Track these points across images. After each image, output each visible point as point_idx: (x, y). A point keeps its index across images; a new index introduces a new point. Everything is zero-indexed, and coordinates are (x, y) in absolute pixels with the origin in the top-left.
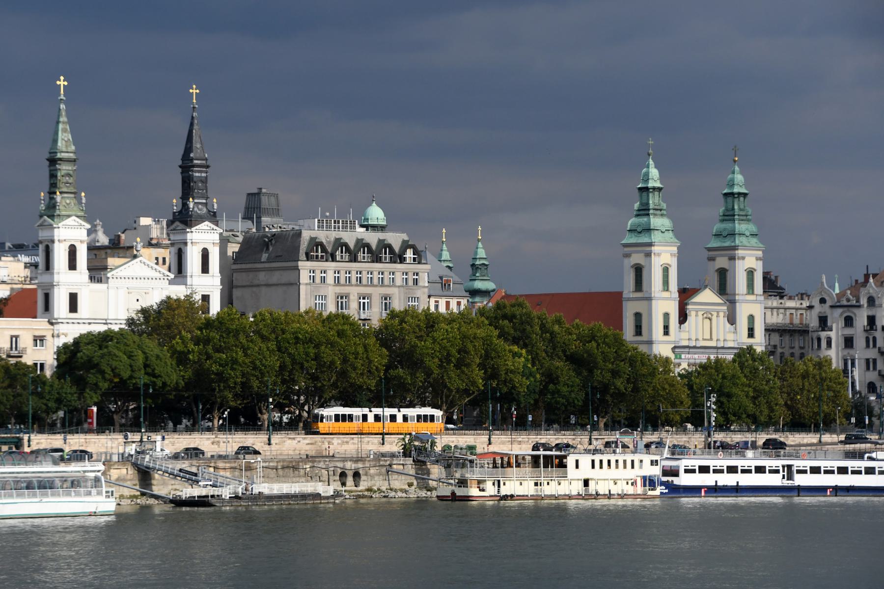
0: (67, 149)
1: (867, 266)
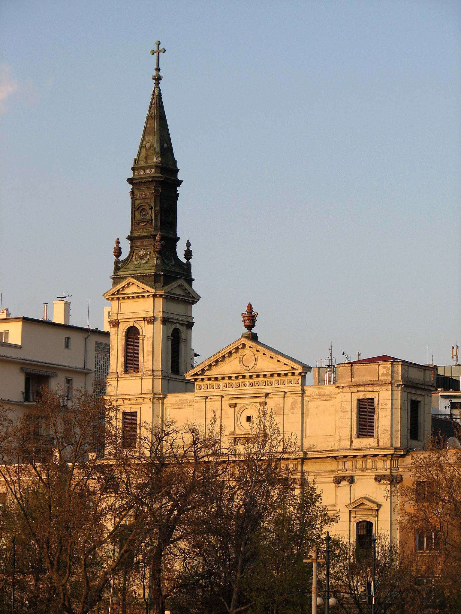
0: (146, 162)
1: (67, 346)
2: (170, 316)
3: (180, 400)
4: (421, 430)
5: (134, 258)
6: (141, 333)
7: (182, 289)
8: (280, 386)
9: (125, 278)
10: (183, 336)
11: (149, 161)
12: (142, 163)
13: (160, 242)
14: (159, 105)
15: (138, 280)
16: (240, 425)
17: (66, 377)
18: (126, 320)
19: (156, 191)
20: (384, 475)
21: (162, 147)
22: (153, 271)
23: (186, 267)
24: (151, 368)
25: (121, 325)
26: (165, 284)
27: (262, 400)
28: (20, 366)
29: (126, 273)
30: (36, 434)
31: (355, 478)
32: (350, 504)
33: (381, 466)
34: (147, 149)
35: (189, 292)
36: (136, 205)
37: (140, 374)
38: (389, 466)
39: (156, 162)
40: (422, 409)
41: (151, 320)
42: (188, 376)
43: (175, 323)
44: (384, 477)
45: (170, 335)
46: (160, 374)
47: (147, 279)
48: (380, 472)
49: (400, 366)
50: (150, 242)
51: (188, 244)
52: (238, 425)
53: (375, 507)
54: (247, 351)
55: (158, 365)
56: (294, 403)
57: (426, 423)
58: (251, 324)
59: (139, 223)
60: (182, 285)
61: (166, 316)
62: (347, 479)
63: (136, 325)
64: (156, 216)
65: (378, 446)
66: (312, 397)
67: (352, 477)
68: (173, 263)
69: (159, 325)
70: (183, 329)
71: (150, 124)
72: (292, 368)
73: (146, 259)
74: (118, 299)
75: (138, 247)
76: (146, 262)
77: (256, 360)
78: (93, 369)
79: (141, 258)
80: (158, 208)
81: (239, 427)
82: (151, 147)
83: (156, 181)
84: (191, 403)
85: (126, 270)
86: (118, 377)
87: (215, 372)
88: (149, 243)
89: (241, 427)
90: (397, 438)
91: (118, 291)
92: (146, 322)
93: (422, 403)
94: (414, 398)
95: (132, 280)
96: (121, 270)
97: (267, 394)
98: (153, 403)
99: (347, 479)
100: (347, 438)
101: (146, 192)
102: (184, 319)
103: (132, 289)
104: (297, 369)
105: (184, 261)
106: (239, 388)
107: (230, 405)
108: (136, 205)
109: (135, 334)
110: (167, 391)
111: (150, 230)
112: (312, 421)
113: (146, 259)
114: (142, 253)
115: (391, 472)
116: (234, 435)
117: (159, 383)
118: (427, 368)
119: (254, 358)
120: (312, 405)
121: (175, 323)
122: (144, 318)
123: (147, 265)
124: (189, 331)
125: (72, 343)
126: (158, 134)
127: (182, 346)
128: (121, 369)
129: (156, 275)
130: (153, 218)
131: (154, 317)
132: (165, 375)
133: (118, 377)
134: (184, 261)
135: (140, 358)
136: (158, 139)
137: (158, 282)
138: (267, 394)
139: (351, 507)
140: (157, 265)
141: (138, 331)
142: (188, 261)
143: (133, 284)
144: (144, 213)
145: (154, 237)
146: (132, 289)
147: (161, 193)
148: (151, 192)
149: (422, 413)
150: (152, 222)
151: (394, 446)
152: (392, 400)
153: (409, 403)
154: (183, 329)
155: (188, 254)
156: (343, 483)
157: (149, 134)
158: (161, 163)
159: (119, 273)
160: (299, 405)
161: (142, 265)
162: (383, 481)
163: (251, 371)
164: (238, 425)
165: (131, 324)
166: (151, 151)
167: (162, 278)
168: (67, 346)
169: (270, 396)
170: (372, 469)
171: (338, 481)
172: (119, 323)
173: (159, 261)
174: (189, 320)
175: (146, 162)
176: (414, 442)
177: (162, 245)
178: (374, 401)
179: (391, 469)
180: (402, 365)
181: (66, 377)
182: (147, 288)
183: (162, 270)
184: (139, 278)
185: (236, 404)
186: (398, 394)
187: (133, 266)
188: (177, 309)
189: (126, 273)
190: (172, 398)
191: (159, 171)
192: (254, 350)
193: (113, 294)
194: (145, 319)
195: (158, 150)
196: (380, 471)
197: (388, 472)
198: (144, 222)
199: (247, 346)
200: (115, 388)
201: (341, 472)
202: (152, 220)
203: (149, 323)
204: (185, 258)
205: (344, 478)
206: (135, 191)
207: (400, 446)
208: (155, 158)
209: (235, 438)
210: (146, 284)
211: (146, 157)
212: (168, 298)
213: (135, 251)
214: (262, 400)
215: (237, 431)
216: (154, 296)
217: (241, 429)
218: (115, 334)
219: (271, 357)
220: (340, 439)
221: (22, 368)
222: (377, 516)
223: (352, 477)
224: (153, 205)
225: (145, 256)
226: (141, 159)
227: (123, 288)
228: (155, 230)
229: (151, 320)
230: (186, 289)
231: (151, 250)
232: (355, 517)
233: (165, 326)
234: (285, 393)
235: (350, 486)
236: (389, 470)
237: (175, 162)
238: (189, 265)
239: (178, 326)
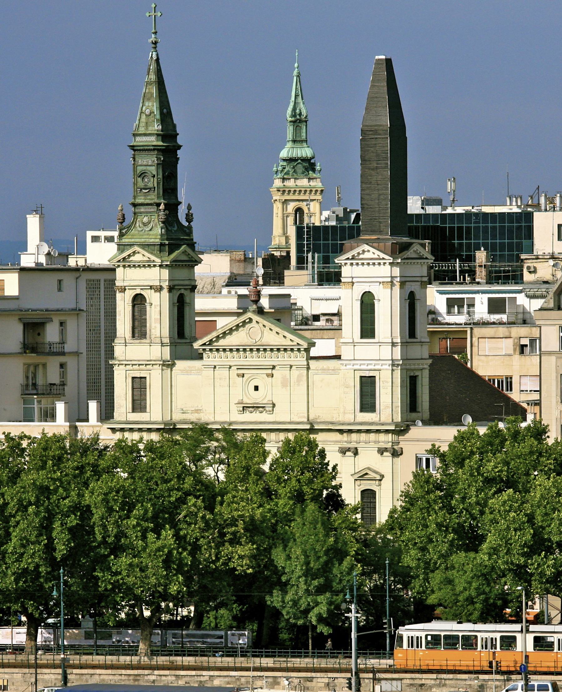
0: (147, 129)
1: (60, 290)
2: (176, 283)
3: (189, 367)
4: (419, 400)
5: (137, 225)
6: (148, 301)
7: (186, 255)
8: (286, 359)
9: (131, 245)
10: (187, 300)
11: (150, 128)
12: (143, 129)
13: (164, 211)
14: (158, 69)
15: (143, 249)
16: (248, 394)
17: (60, 320)
18: (133, 287)
19: (158, 159)
20: (386, 448)
21: (161, 113)
22: (158, 241)
23: (188, 231)
24: (158, 335)
25: (127, 291)
26: (170, 253)
27: (269, 371)
28: (17, 318)
29: (130, 240)
30: (34, 385)
31: (359, 451)
32: (355, 473)
33: (383, 440)
34: (146, 115)
35: (192, 257)
36: (138, 172)
37: (148, 341)
38: (390, 440)
39: (158, 130)
40: (420, 382)
41: (160, 289)
42: (196, 345)
43: (180, 289)
44: (386, 450)
45: (176, 301)
46: (168, 342)
47: (152, 247)
48: (383, 445)
49: (399, 347)
50: (154, 209)
51: (189, 207)
52: (245, 394)
53: (378, 477)
54: (254, 324)
55: (166, 332)
56: (299, 376)
57: (423, 403)
58: (257, 299)
59: (141, 189)
60: (185, 251)
61: (172, 283)
62: (352, 450)
63: (143, 292)
64: (158, 183)
65: (380, 420)
66: (317, 371)
67: (356, 449)
68: (176, 228)
69: (165, 294)
70: (186, 293)
71: (149, 89)
72: (298, 344)
73: (150, 226)
74: (124, 266)
75: (141, 213)
76: (151, 230)
77: (262, 333)
78: (85, 310)
79: (145, 224)
80: (160, 176)
81: (246, 395)
82: (151, 113)
83: (158, 150)
84: (200, 370)
85: (130, 237)
86: (126, 343)
87: (222, 343)
88: (152, 210)
89: (248, 394)
90: (397, 414)
91: (124, 259)
92: (153, 291)
93: (420, 377)
94: (412, 374)
95: (136, 248)
96: (124, 237)
97: (274, 367)
98: (162, 370)
99: (352, 450)
100: (351, 412)
101: (148, 160)
102: (187, 283)
103: (137, 258)
104: (302, 346)
105: (186, 224)
106: (246, 359)
107: (238, 375)
108: (138, 172)
109: (141, 301)
110: (176, 356)
111: (153, 198)
112: (317, 394)
113: (150, 226)
114: (145, 220)
115: (392, 445)
116: (242, 403)
117: (167, 350)
118: (424, 344)
119: (260, 331)
120: (315, 377)
121: (180, 289)
122: (151, 286)
123: (151, 233)
124: (192, 294)
125: (65, 284)
126: (158, 100)
127: (187, 310)
128: (128, 334)
129: (162, 245)
130: (156, 185)
131: (161, 286)
132: (173, 341)
133: (126, 343)
134: (186, 224)
135: (148, 325)
136: (158, 106)
137: (163, 251)
138: (274, 367)
139: (356, 477)
140: (162, 235)
141: (145, 298)
142: (189, 224)
143: (138, 253)
144: (146, 180)
145: (158, 205)
146: (137, 258)
147: (163, 161)
148: (153, 159)
149: (420, 386)
150: (154, 190)
151: (395, 421)
152: (392, 378)
153: (408, 380)
154: (186, 293)
155: (189, 218)
156: (348, 454)
157: (149, 100)
158: (162, 131)
159: (123, 240)
160: (305, 378)
161: (147, 232)
162: (385, 454)
163: (257, 344)
164: (245, 394)
165: (138, 291)
166: (151, 118)
167: (167, 247)
168: (60, 290)
169: (277, 368)
170: (375, 442)
171: (343, 451)
172: (125, 289)
173: (163, 230)
174: (193, 284)
175: (147, 129)
176: (414, 415)
177: (166, 215)
178: (362, 190)
179: (393, 443)
180: (401, 370)
181: (60, 320)
182: (153, 258)
183: (167, 239)
184: (145, 246)
185: (243, 374)
186: (398, 373)
187: (137, 232)
188: (182, 274)
189: (130, 240)
190: (180, 364)
191: (160, 138)
192: (261, 325)
193: (119, 261)
194: (151, 287)
195: (158, 117)
196: (383, 444)
197: (389, 445)
198: (146, 189)
199: (254, 321)
200: (123, 353)
201: (346, 444)
202: (155, 188)
203: (155, 291)
204: (187, 221)
205: (349, 450)
206: (136, 156)
207: (400, 421)
208: (156, 126)
209: (244, 407)
210: (152, 253)
211: (147, 123)
212: (174, 266)
213: (139, 217)
214: (269, 371)
215: (246, 400)
216: (161, 266)
217: (249, 398)
218: (121, 300)
219: (277, 333)
220: (344, 413)
221: (20, 319)
222: (380, 485)
223: (356, 449)
224: (155, 173)
225: (149, 222)
226: (141, 125)
227: (129, 256)
228: (158, 198)
229: (160, 289)
230: (189, 254)
231: (155, 218)
232: (359, 486)
233: (171, 294)
234: (291, 366)
235: (355, 457)
236: (391, 444)
237: (174, 126)
238: (190, 228)
239: (182, 291)
